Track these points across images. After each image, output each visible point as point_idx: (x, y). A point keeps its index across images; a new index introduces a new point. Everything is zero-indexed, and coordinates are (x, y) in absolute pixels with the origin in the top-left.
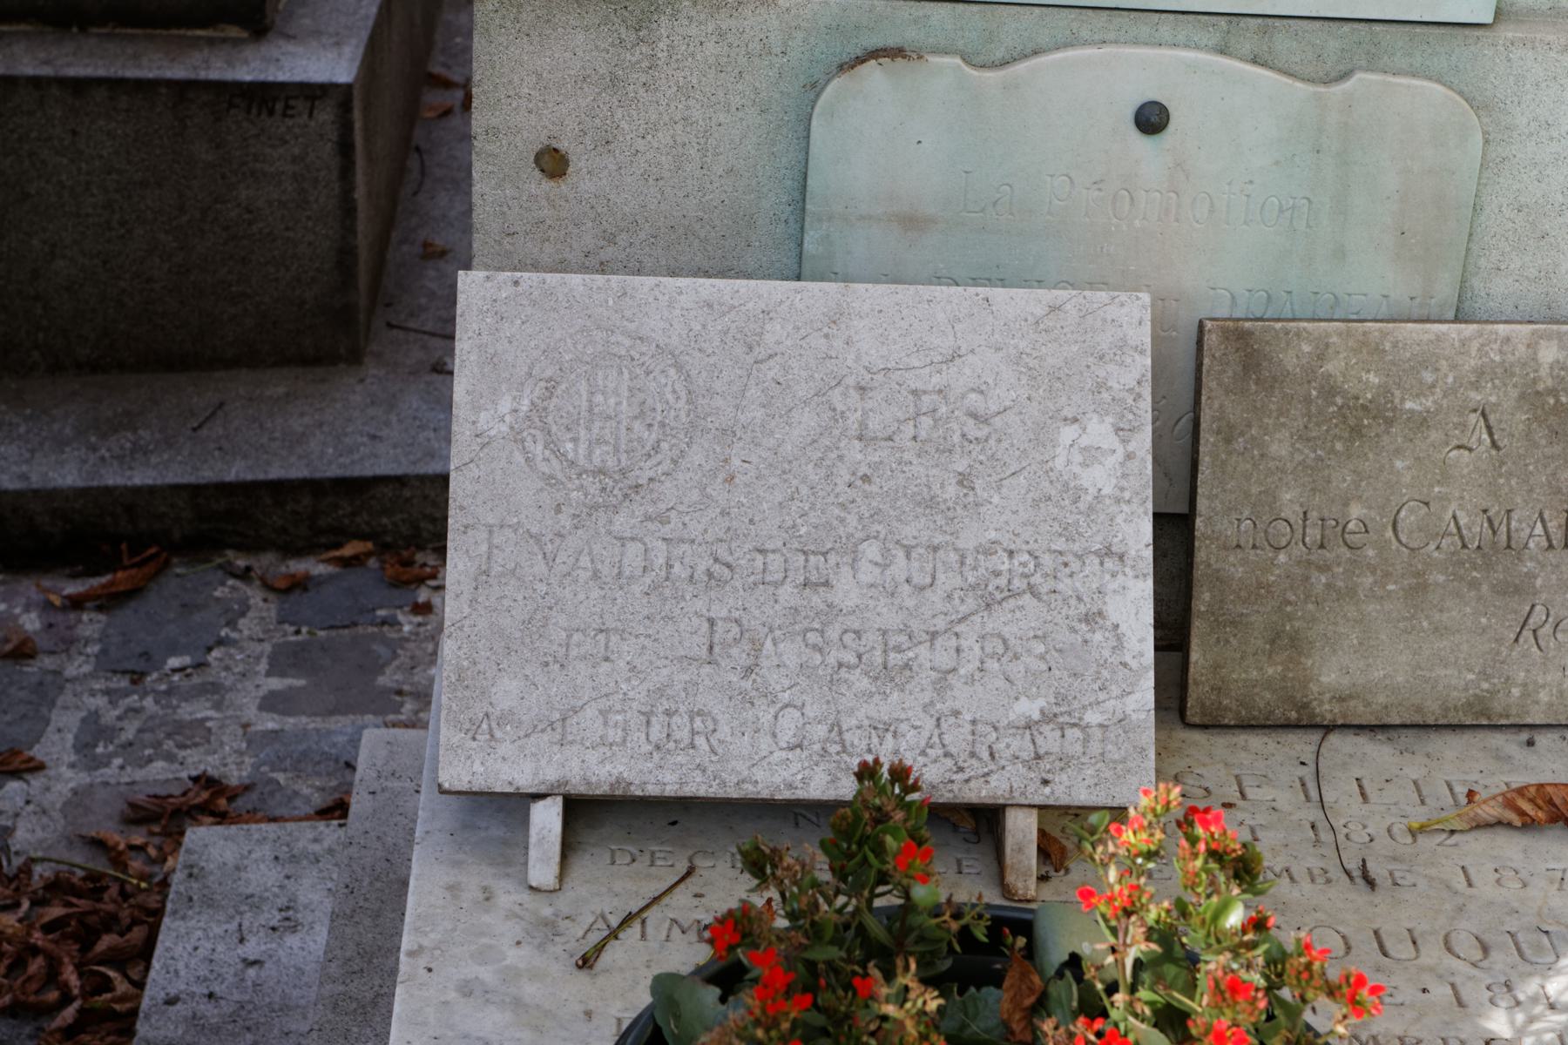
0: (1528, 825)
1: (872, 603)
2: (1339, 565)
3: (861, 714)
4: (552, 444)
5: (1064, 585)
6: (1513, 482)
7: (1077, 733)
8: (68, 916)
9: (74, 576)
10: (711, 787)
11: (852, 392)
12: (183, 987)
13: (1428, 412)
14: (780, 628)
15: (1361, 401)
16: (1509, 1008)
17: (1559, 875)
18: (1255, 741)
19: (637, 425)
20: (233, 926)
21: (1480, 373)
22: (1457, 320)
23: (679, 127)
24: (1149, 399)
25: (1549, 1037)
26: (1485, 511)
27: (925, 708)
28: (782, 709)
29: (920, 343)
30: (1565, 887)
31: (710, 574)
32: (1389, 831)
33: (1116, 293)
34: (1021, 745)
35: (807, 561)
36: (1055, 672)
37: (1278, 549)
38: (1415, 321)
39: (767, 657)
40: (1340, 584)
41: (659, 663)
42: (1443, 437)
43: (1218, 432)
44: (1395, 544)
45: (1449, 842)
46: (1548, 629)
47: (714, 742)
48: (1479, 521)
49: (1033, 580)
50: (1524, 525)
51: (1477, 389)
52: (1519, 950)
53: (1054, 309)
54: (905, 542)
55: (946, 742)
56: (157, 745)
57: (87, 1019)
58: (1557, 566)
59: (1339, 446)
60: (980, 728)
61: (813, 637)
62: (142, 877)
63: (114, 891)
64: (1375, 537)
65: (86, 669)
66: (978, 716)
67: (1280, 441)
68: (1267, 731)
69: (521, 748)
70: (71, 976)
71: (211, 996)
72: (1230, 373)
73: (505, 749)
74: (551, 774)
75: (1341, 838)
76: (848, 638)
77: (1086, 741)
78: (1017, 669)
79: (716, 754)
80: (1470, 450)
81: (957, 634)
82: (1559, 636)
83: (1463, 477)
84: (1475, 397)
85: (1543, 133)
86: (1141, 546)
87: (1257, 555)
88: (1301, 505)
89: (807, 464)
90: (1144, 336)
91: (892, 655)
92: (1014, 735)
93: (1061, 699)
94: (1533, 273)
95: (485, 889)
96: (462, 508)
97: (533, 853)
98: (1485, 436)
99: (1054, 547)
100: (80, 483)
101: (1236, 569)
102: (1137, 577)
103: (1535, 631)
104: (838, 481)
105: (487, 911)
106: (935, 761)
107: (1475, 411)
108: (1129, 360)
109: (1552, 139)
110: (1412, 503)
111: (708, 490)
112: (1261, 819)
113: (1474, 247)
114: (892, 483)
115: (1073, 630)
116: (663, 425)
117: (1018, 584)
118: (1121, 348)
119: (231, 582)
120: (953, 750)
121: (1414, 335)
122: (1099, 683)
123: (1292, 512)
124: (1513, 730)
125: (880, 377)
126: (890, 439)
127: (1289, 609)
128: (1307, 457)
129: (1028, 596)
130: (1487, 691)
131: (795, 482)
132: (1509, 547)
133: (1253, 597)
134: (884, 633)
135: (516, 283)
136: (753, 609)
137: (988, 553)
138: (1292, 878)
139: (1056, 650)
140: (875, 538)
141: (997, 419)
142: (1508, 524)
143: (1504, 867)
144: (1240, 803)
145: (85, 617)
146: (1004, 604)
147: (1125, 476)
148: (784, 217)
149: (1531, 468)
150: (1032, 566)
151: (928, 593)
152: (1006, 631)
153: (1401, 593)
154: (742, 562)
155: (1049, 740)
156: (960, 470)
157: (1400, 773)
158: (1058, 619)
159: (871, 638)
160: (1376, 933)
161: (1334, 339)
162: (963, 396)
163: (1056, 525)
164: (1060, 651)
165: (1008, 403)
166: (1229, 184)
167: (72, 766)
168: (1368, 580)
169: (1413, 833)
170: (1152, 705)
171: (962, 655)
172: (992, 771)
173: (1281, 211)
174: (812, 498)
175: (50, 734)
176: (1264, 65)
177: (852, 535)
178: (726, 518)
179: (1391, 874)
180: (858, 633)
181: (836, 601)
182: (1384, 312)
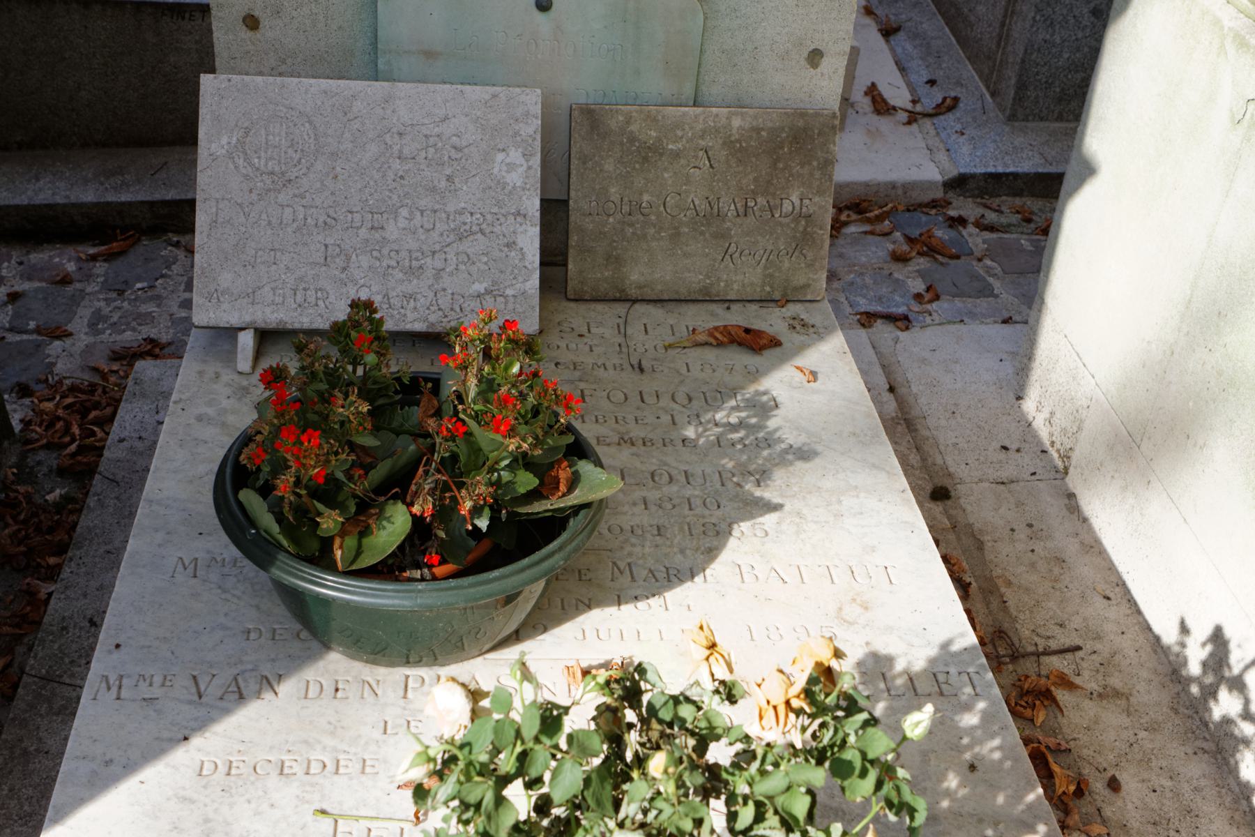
0: (720, 344)
3: (398, 290)
4: (247, 159)
5: (497, 229)
7: (502, 299)
8: (75, 402)
9: (94, 245)
11: (396, 136)
12: (127, 434)
16: (696, 426)
18: (600, 307)
19: (290, 151)
20: (154, 406)
21: (704, 131)
22: (694, 105)
23: (313, 5)
25: (712, 438)
31: (325, 223)
37: (609, 216)
40: (639, 232)
41: (300, 265)
43: (580, 159)
44: (665, 214)
46: (737, 255)
53: (494, 96)
56: (128, 324)
57: (81, 450)
60: (456, 297)
61: (375, 253)
62: (116, 385)
63: (100, 391)
65: (96, 288)
69: (233, 306)
70: (76, 430)
71: (140, 438)
73: (225, 306)
74: (248, 318)
75: (631, 350)
76: (393, 254)
77: (506, 303)
78: (474, 269)
84: (702, 143)
91: (414, 262)
93: (494, 283)
95: (216, 373)
96: (203, 190)
97: (239, 356)
100: (95, 200)
105: (215, 383)
112: (595, 342)
115: (501, 251)
116: (302, 151)
117: (475, 228)
119: (169, 248)
120: (442, 307)
123: (615, 198)
125: (409, 129)
129: (479, 235)
134: (410, 251)
135: (229, 80)
137: (461, 214)
138: (605, 368)
144: (587, 335)
145: (98, 265)
151: (431, 232)
152: (469, 251)
155: (489, 303)
158: (494, 245)
159: (404, 254)
160: (641, 392)
161: (634, 114)
162: (450, 138)
167: (86, 334)
168: (652, 231)
169: (666, 348)
170: (538, 286)
175: (77, 319)
180: (397, 252)
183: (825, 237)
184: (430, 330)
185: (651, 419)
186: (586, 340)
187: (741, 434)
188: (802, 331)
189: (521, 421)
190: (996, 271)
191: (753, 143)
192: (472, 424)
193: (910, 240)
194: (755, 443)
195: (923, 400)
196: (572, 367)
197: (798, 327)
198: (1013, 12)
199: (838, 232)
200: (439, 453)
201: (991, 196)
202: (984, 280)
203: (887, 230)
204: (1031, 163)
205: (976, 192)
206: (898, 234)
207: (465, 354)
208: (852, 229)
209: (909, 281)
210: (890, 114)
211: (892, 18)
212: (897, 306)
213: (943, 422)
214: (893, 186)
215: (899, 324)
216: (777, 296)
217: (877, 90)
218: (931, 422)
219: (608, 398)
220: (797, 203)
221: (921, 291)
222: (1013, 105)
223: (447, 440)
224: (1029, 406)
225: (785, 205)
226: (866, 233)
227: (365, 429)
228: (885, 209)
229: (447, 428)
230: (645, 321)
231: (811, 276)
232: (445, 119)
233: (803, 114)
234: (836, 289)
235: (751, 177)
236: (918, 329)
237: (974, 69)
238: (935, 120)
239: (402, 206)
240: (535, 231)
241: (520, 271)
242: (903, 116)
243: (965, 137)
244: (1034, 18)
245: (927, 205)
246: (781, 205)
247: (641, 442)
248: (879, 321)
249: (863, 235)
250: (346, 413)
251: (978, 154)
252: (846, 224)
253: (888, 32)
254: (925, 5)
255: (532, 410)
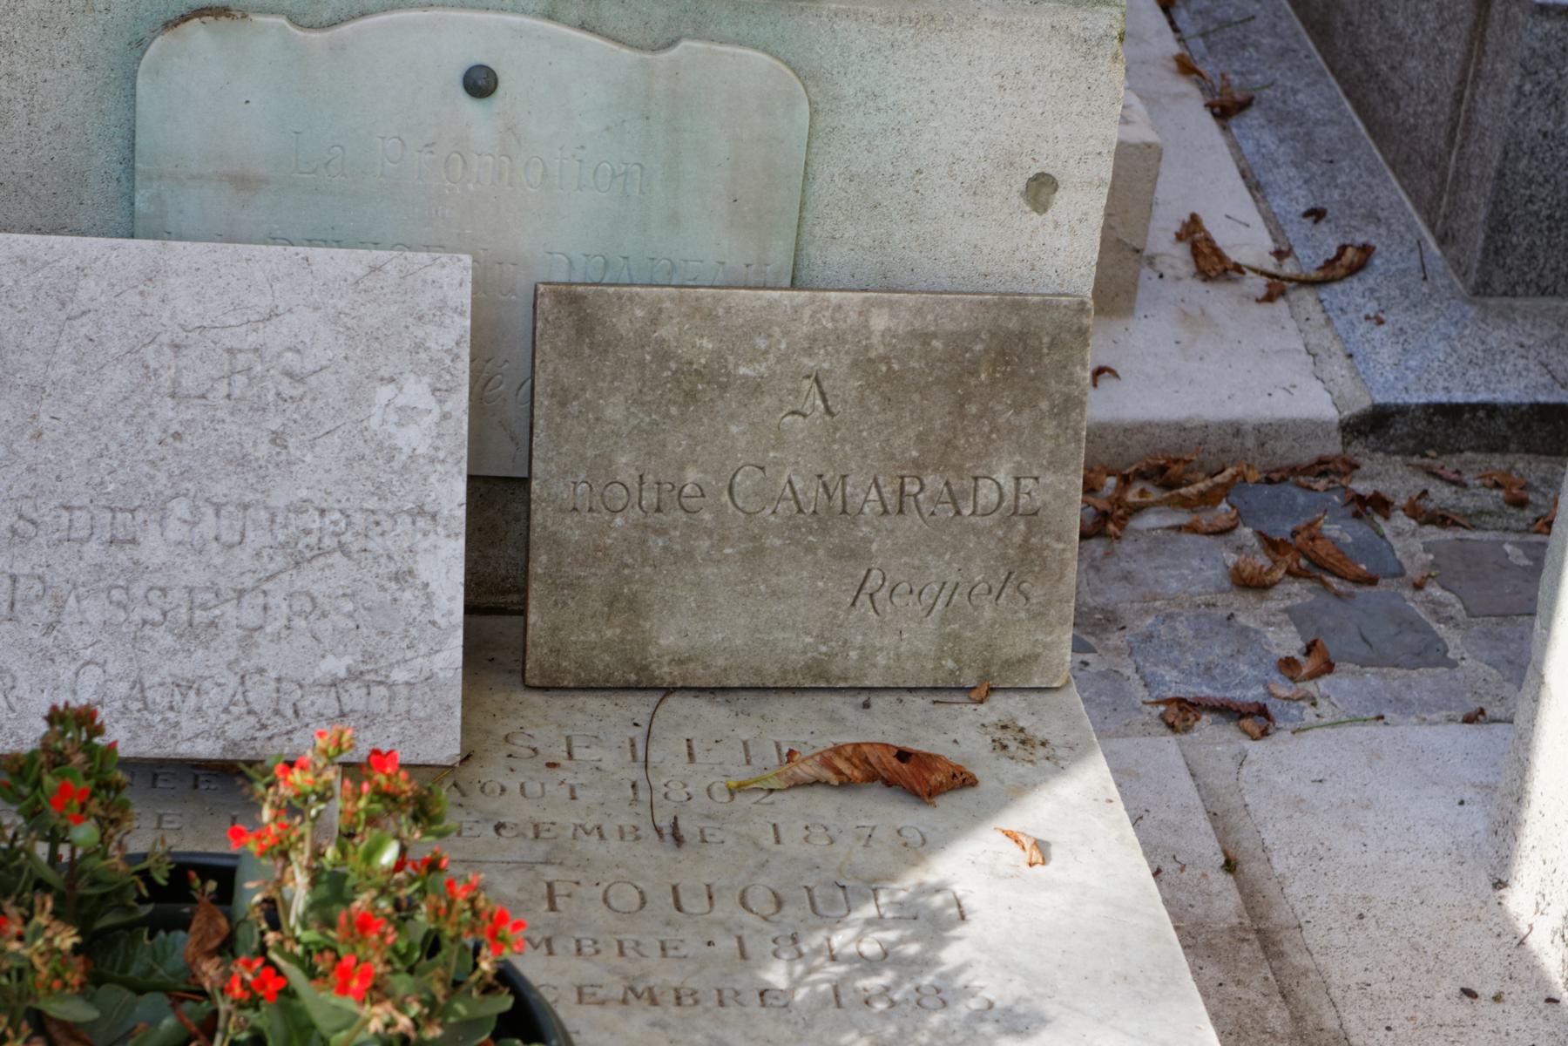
0: (846, 784)
1: (179, 561)
2: (675, 528)
3: (164, 671)
5: (375, 544)
6: (847, 447)
7: (383, 690)
10: (7, 744)
11: (166, 350)
13: (762, 377)
14: (84, 585)
15: (695, 366)
16: (791, 960)
17: (868, 832)
18: (593, 703)
22: (793, 286)
24: (467, 360)
25: (823, 987)
26: (820, 476)
27: (230, 665)
28: (83, 666)
29: (237, 301)
30: (871, 843)
32: (709, 790)
33: (438, 255)
34: (325, 702)
35: (114, 518)
36: (364, 630)
38: (750, 288)
39: (70, 614)
40: (677, 547)
42: (777, 403)
43: (553, 396)
44: (731, 508)
45: (765, 801)
46: (884, 593)
47: (12, 699)
48: (814, 485)
49: (343, 539)
50: (859, 490)
51: (810, 356)
52: (813, 904)
53: (374, 269)
54: (215, 500)
55: (250, 700)
58: (892, 531)
59: (674, 410)
60: (285, 685)
64: (712, 501)
66: (283, 674)
67: (615, 405)
68: (607, 693)
72: (564, 337)
75: (658, 797)
76: (153, 596)
77: (392, 699)
78: (324, 627)
79: (14, 711)
80: (805, 416)
81: (265, 593)
82: (895, 600)
83: (797, 442)
84: (808, 363)
85: (870, 104)
86: (454, 505)
87: (593, 518)
88: (637, 469)
89: (117, 421)
90: (465, 297)
91: (198, 613)
92: (320, 693)
93: (368, 656)
94: (867, 242)
98: (819, 402)
99: (366, 506)
101: (572, 531)
102: (449, 536)
103: (871, 595)
104: (149, 438)
106: (238, 718)
107: (808, 377)
108: (448, 321)
109: (879, 110)
110: (747, 468)
111: (14, 446)
112: (582, 778)
113: (808, 215)
114: (204, 440)
115: (383, 589)
117: (328, 542)
118: (440, 309)
120: (257, 708)
121: (746, 301)
122: (407, 641)
123: (628, 476)
124: (852, 693)
125: (195, 335)
126: (203, 397)
127: (626, 571)
128: (642, 421)
129: (338, 555)
130: (825, 654)
131: (104, 439)
132: (844, 512)
133: (590, 560)
134: (191, 590)
136: (56, 566)
137: (299, 511)
138: (602, 836)
139: (365, 609)
140: (185, 495)
141: (312, 378)
142: (843, 490)
143: (814, 825)
144: (565, 763)
146: (314, 562)
147: (440, 436)
148: (115, 176)
149: (865, 434)
150: (343, 524)
151: (237, 551)
152: (314, 589)
153: (738, 557)
154: (47, 519)
155: (355, 697)
156: (273, 429)
157: (731, 733)
159: (177, 595)
160: (675, 888)
161: (667, 304)
162: (279, 355)
163: (369, 484)
164: (369, 609)
165: (324, 363)
166: (561, 149)
168: (705, 544)
170: (459, 662)
171: (270, 613)
172: (295, 729)
173: (614, 176)
174: (121, 456)
176: (592, 31)
177: (161, 493)
178: (32, 475)
179: (702, 832)
181: (143, 559)
182: (720, 278)
183: (1068, 555)
184: (230, 757)
185: (693, 946)
186: (560, 774)
187: (886, 978)
188: (1021, 753)
189: (398, 965)
190: (1451, 611)
191: (913, 364)
192: (295, 975)
193: (1272, 545)
194: (913, 998)
195: (1295, 890)
196: (531, 834)
197: (1013, 746)
198: (1478, 74)
199: (1122, 528)
200: (225, 1032)
201: (1442, 451)
202: (1427, 629)
203: (1222, 523)
204: (1523, 382)
205: (1411, 443)
206: (1245, 533)
207: (282, 826)
208: (1150, 520)
209: (1270, 634)
210: (1230, 280)
211: (1235, 80)
212: (1243, 685)
213: (1338, 938)
214: (1237, 429)
215: (1247, 723)
216: (969, 678)
217: (1202, 229)
218: (1314, 936)
219: (605, 900)
220: (1009, 487)
221: (1409, 573)
222: (1482, 263)
223: (241, 1007)
224: (1519, 901)
225: (983, 491)
226: (1179, 528)
227: (66, 985)
228: (1218, 479)
229: (243, 981)
230: (689, 734)
231: (1040, 637)
232: (271, 315)
233: (1017, 304)
234: (1116, 648)
235: (912, 434)
236: (1287, 735)
237: (1404, 187)
238: (1324, 293)
239: (177, 496)
240: (456, 548)
241: (422, 630)
242: (1258, 285)
243: (1384, 328)
244: (1519, 88)
245: (1307, 470)
246: (975, 490)
247: (671, 997)
248: (1206, 718)
249: (1173, 533)
250: (26, 952)
251: (1412, 363)
252: (1137, 509)
253: (1225, 111)
254: (1302, 54)
255: (423, 944)
